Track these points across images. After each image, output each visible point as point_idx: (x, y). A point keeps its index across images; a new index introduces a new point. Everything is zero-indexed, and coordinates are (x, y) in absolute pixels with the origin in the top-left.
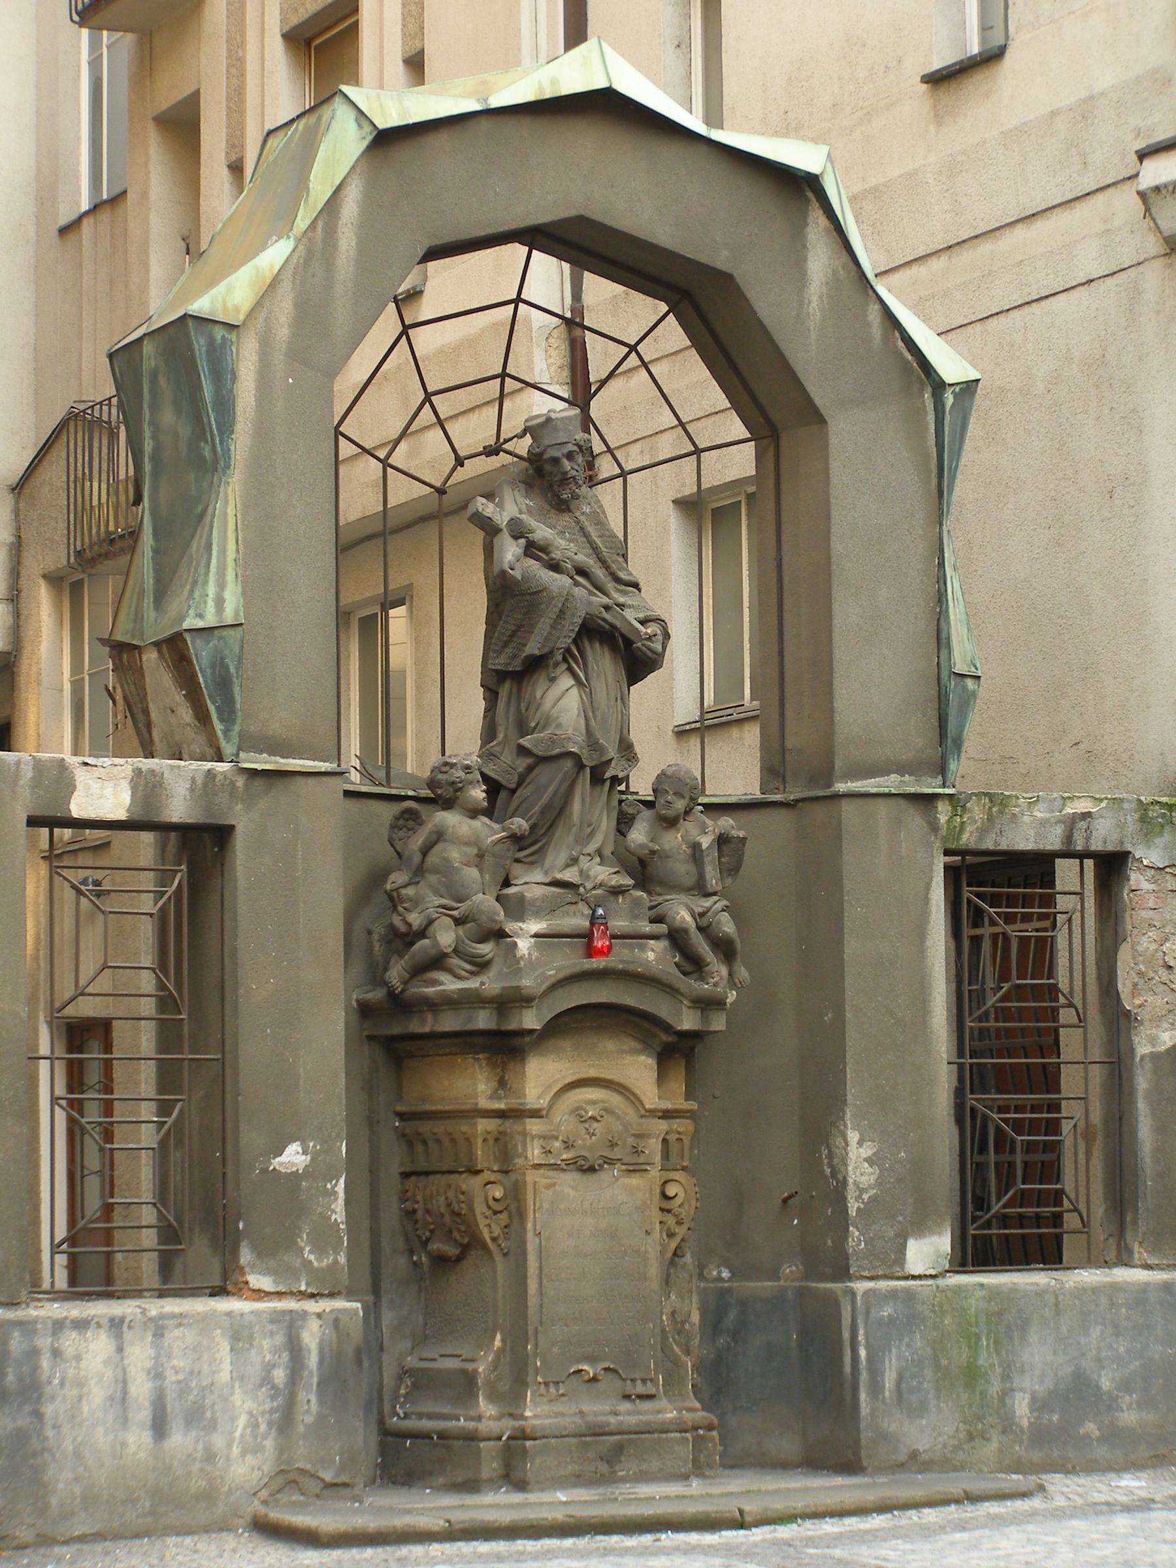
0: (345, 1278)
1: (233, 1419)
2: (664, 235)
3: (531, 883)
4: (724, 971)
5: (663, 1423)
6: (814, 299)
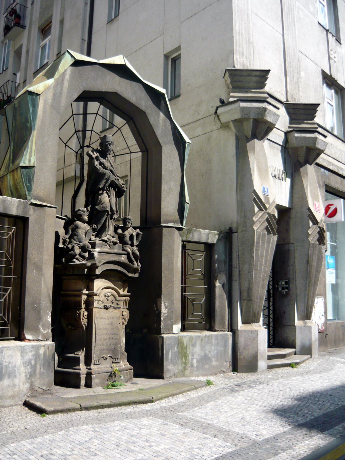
1: (20, 374)
5: (122, 369)
6: (161, 120)
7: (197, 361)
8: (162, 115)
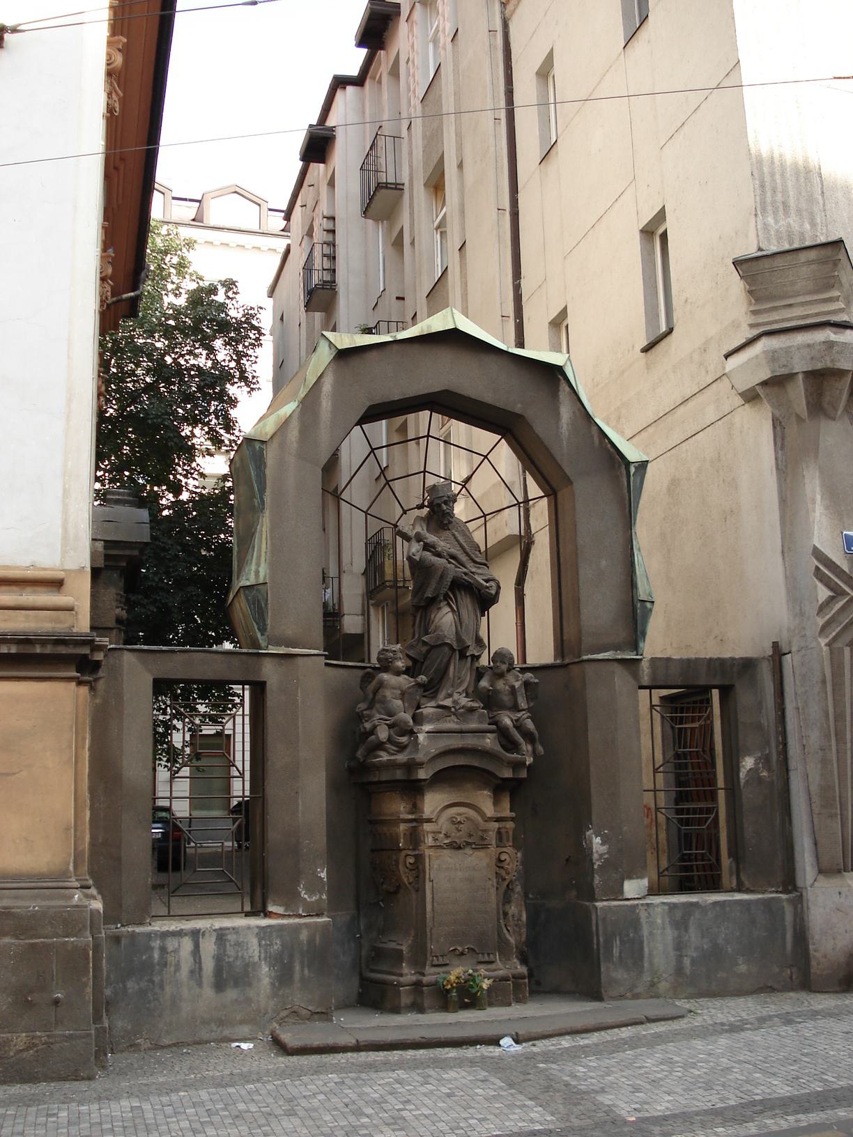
0: (325, 905)
2: (488, 397)
3: (428, 709)
4: (530, 748)
7: (693, 962)
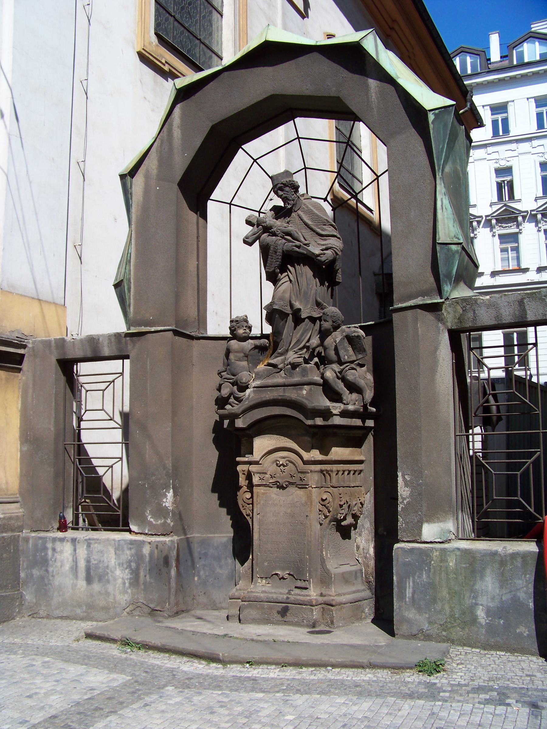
1: (115, 580)
7: (489, 612)
8: (373, 83)
